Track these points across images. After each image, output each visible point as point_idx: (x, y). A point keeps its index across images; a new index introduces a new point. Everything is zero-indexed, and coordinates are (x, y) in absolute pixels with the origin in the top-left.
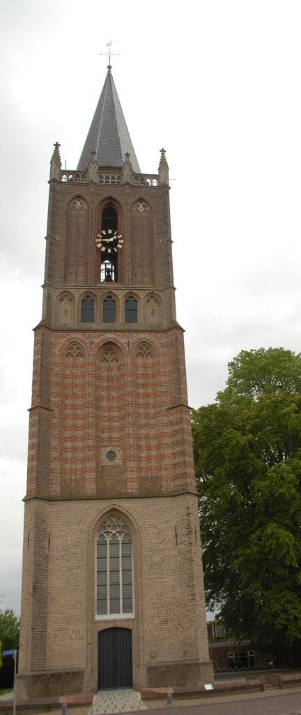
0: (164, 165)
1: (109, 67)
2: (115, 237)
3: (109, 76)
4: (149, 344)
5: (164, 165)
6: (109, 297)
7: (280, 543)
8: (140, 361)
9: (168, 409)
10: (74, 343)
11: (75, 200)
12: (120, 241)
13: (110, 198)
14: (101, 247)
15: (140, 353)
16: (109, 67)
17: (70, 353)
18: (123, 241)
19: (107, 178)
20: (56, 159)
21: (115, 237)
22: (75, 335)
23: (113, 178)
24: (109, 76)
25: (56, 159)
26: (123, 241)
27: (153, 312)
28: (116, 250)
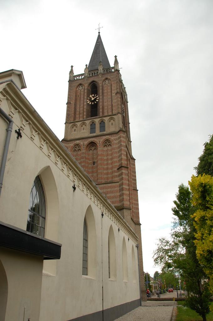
0: (116, 62)
1: (99, 33)
2: (95, 97)
3: (99, 37)
4: (109, 140)
5: (116, 62)
6: (93, 123)
7: (175, 262)
8: (105, 149)
9: (118, 169)
10: (78, 145)
11: (105, 80)
12: (97, 98)
13: (93, 81)
14: (89, 103)
15: (105, 145)
16: (99, 33)
17: (75, 150)
18: (98, 98)
19: (92, 74)
20: (71, 72)
21: (95, 97)
22: (78, 142)
23: (95, 73)
24: (99, 37)
25: (71, 72)
26: (98, 98)
27: (112, 124)
28: (95, 102)
